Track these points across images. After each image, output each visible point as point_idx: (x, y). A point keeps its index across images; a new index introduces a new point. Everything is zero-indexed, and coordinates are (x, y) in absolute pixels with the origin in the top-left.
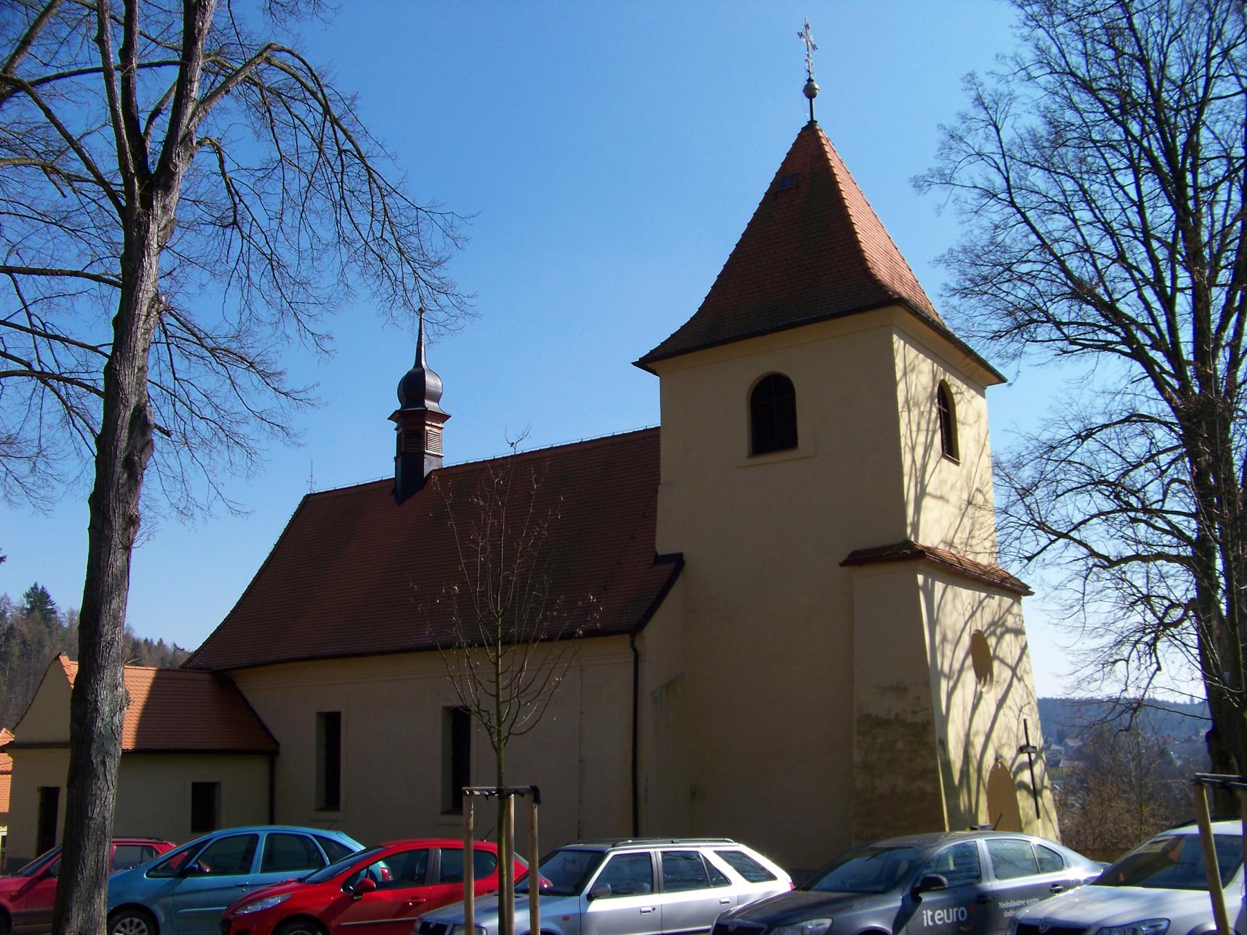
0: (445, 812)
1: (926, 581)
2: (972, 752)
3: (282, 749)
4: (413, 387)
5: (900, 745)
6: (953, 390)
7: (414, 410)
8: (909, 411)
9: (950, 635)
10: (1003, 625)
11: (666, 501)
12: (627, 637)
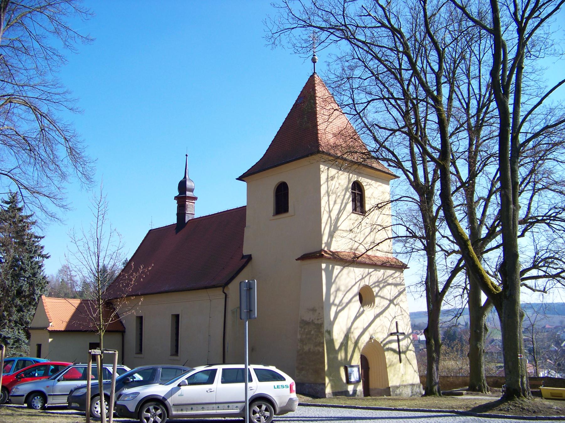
0: (137, 353)
1: (327, 267)
2: (351, 336)
3: (126, 330)
4: (182, 186)
5: (313, 332)
6: (364, 184)
7: (183, 196)
8: (329, 196)
9: (342, 288)
10: (386, 282)
11: (248, 233)
12: (221, 289)
